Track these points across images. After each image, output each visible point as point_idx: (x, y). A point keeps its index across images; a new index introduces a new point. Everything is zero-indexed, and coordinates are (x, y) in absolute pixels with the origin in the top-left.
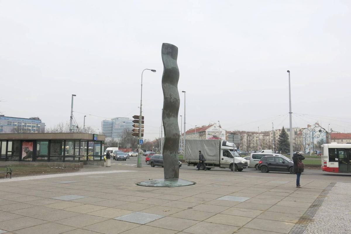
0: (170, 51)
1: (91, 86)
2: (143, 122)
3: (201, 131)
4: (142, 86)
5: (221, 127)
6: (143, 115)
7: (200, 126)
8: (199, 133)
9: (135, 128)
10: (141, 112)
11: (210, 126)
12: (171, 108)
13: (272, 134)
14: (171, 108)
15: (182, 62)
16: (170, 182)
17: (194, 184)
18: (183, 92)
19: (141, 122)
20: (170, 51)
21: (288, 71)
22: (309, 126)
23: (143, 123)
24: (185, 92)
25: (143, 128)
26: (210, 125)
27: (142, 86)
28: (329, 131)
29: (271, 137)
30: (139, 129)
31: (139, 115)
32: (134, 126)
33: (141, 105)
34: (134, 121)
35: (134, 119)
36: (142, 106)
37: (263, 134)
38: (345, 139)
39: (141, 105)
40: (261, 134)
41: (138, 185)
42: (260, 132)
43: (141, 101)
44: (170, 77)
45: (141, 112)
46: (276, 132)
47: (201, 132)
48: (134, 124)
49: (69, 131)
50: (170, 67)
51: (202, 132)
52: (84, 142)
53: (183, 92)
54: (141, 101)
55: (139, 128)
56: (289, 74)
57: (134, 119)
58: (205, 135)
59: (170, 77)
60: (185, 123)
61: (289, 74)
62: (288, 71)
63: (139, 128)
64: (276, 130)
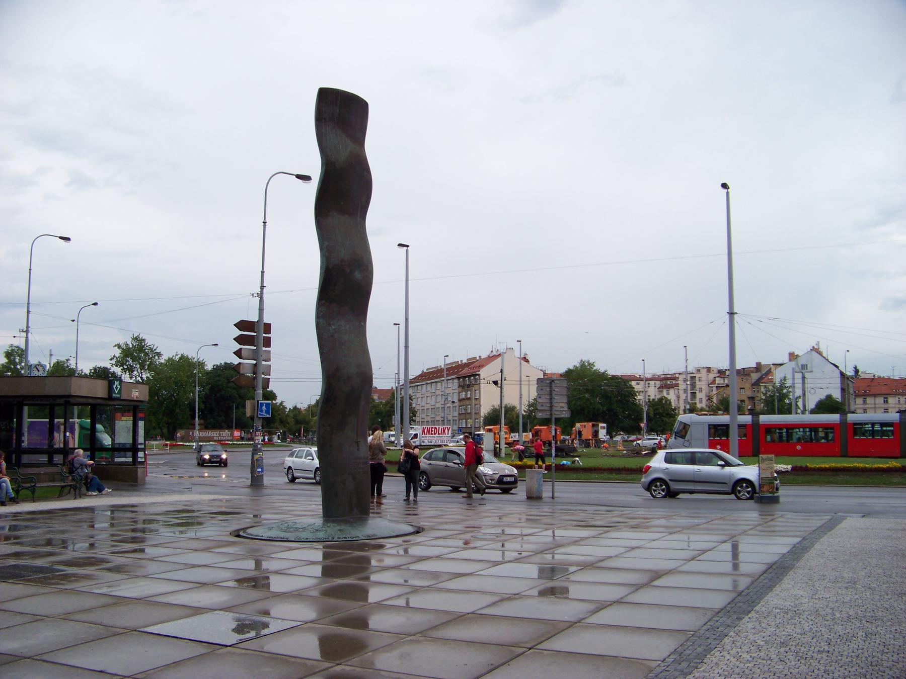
0: (341, 115)
1: (182, 252)
2: (267, 342)
3: (465, 371)
4: (264, 226)
5: (527, 361)
6: (266, 320)
7: (461, 356)
8: (459, 378)
9: (241, 361)
10: (261, 310)
11: (491, 358)
12: (344, 287)
13: (685, 380)
14: (344, 287)
15: (378, 146)
16: (338, 528)
17: (418, 532)
18: (400, 245)
19: (261, 342)
20: (341, 115)
21: (724, 186)
22: (793, 356)
23: (269, 346)
24: (408, 246)
25: (269, 360)
26: (494, 353)
27: (264, 226)
28: (850, 372)
29: (681, 392)
30: (255, 365)
31: (254, 318)
32: (238, 353)
33: (262, 287)
34: (239, 339)
35: (238, 333)
36: (265, 290)
37: (658, 383)
38: (895, 395)
39: (262, 287)
40: (652, 383)
41: (239, 536)
42: (649, 376)
43: (263, 272)
44: (343, 192)
45: (261, 310)
46: (697, 376)
47: (464, 377)
48: (238, 346)
49: (318, 490)
50: (342, 157)
51: (469, 376)
52: (76, 407)
53: (400, 245)
54: (263, 272)
55: (254, 362)
56: (728, 193)
57: (238, 333)
58: (476, 387)
59: (343, 192)
60: (406, 347)
61: (728, 193)
62: (724, 186)
63: (254, 362)
64: (699, 371)
